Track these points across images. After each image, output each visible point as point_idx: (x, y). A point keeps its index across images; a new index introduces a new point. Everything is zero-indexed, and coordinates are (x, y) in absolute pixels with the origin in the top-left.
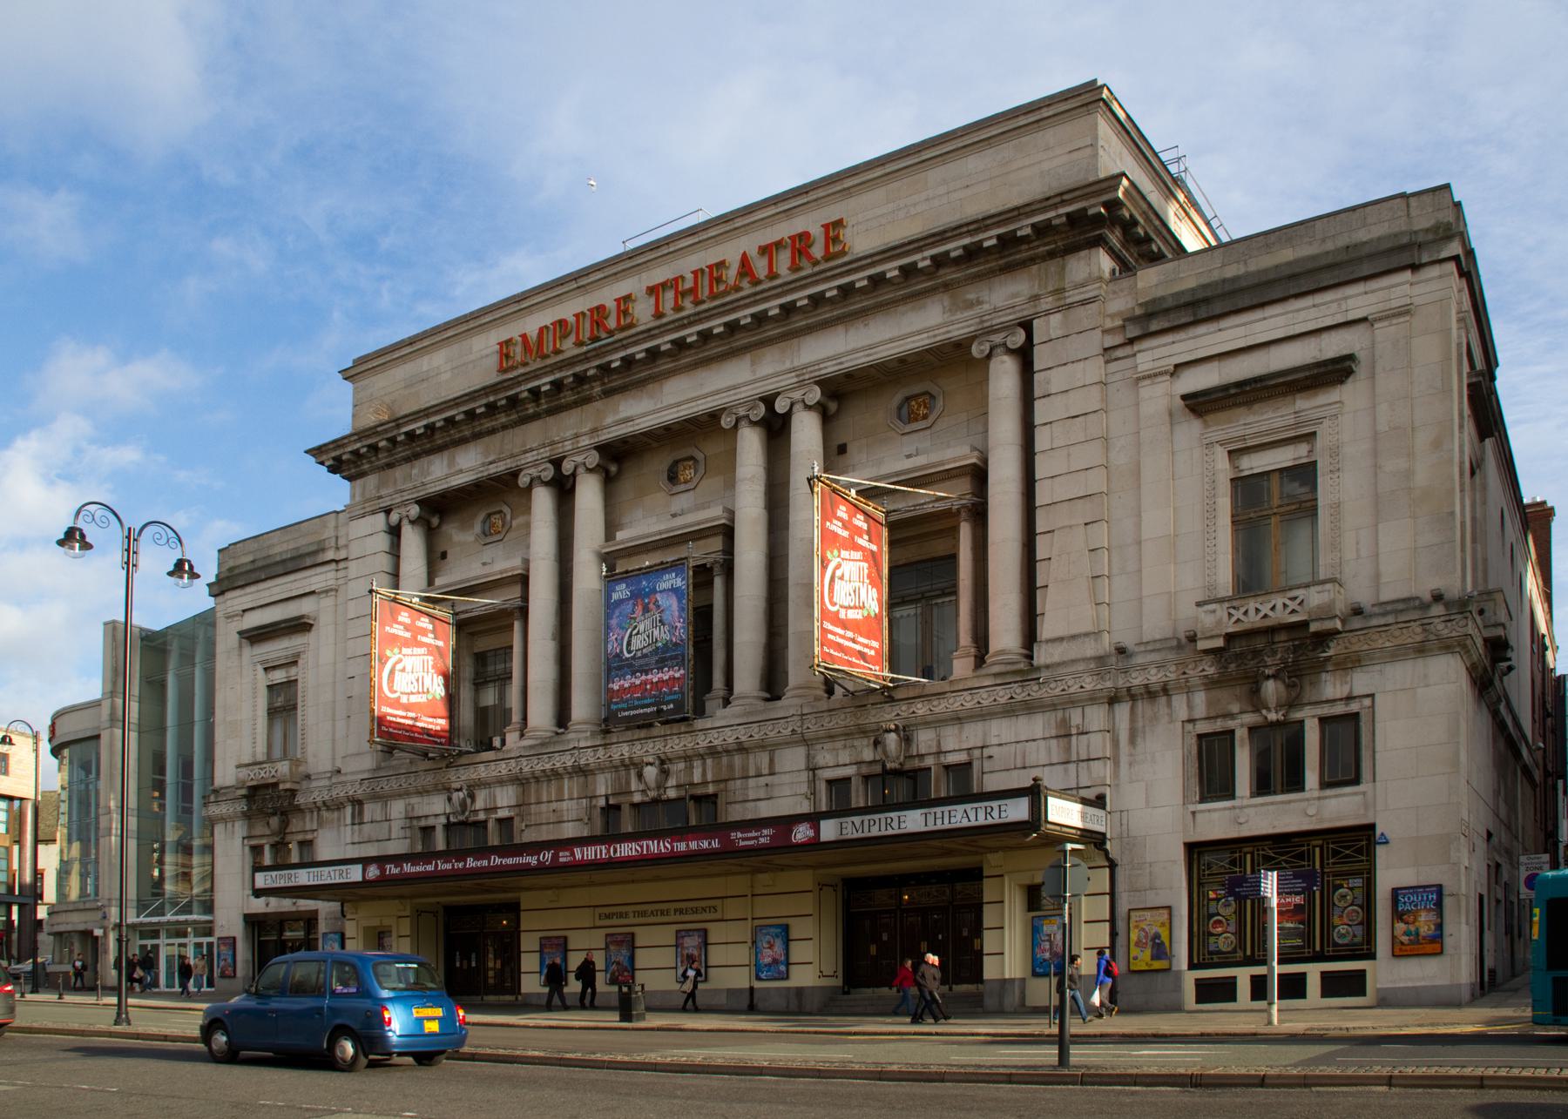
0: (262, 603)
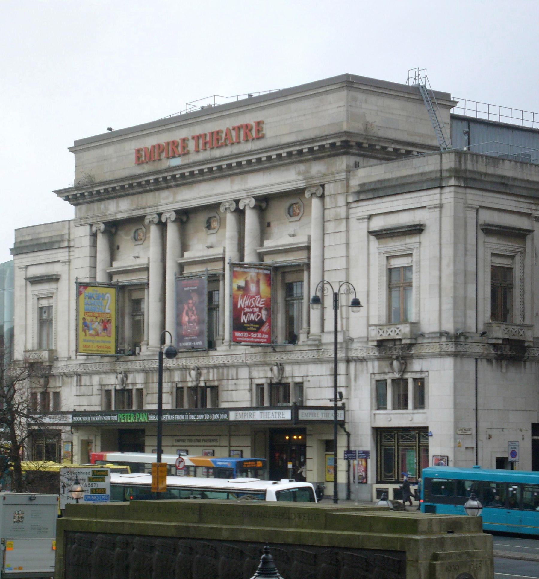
0: (38, 264)
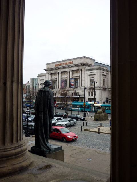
0: (40, 78)
